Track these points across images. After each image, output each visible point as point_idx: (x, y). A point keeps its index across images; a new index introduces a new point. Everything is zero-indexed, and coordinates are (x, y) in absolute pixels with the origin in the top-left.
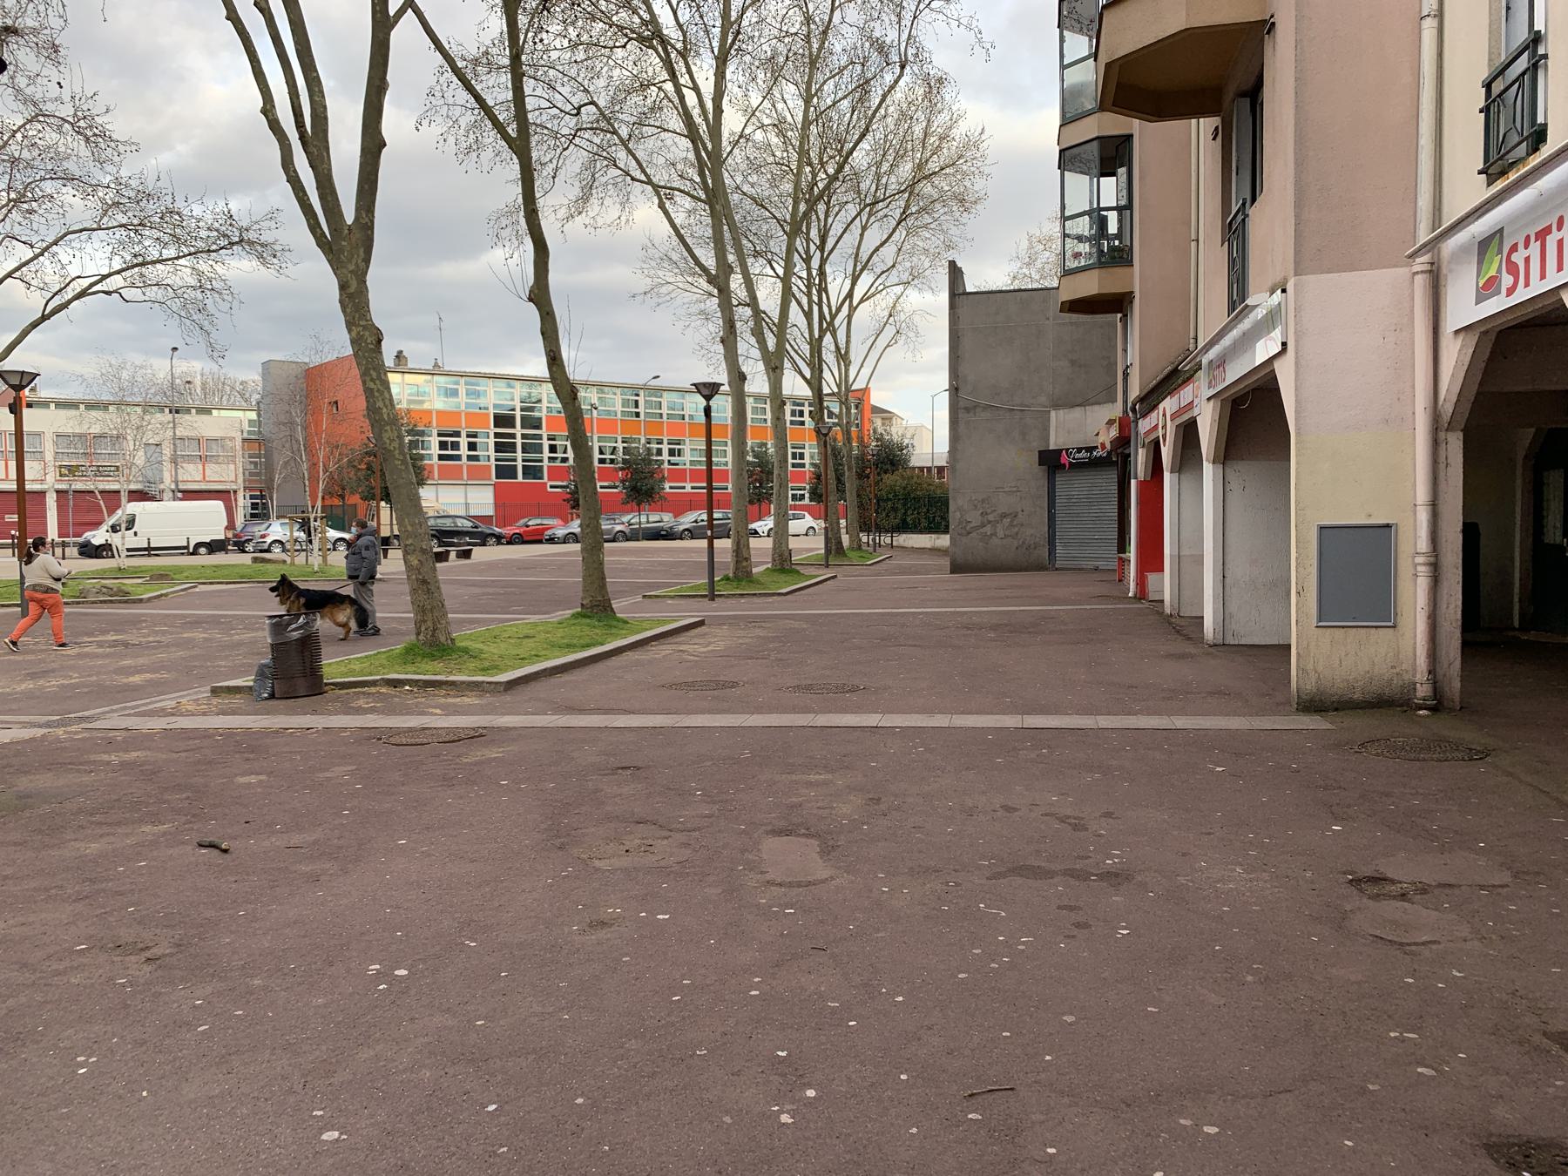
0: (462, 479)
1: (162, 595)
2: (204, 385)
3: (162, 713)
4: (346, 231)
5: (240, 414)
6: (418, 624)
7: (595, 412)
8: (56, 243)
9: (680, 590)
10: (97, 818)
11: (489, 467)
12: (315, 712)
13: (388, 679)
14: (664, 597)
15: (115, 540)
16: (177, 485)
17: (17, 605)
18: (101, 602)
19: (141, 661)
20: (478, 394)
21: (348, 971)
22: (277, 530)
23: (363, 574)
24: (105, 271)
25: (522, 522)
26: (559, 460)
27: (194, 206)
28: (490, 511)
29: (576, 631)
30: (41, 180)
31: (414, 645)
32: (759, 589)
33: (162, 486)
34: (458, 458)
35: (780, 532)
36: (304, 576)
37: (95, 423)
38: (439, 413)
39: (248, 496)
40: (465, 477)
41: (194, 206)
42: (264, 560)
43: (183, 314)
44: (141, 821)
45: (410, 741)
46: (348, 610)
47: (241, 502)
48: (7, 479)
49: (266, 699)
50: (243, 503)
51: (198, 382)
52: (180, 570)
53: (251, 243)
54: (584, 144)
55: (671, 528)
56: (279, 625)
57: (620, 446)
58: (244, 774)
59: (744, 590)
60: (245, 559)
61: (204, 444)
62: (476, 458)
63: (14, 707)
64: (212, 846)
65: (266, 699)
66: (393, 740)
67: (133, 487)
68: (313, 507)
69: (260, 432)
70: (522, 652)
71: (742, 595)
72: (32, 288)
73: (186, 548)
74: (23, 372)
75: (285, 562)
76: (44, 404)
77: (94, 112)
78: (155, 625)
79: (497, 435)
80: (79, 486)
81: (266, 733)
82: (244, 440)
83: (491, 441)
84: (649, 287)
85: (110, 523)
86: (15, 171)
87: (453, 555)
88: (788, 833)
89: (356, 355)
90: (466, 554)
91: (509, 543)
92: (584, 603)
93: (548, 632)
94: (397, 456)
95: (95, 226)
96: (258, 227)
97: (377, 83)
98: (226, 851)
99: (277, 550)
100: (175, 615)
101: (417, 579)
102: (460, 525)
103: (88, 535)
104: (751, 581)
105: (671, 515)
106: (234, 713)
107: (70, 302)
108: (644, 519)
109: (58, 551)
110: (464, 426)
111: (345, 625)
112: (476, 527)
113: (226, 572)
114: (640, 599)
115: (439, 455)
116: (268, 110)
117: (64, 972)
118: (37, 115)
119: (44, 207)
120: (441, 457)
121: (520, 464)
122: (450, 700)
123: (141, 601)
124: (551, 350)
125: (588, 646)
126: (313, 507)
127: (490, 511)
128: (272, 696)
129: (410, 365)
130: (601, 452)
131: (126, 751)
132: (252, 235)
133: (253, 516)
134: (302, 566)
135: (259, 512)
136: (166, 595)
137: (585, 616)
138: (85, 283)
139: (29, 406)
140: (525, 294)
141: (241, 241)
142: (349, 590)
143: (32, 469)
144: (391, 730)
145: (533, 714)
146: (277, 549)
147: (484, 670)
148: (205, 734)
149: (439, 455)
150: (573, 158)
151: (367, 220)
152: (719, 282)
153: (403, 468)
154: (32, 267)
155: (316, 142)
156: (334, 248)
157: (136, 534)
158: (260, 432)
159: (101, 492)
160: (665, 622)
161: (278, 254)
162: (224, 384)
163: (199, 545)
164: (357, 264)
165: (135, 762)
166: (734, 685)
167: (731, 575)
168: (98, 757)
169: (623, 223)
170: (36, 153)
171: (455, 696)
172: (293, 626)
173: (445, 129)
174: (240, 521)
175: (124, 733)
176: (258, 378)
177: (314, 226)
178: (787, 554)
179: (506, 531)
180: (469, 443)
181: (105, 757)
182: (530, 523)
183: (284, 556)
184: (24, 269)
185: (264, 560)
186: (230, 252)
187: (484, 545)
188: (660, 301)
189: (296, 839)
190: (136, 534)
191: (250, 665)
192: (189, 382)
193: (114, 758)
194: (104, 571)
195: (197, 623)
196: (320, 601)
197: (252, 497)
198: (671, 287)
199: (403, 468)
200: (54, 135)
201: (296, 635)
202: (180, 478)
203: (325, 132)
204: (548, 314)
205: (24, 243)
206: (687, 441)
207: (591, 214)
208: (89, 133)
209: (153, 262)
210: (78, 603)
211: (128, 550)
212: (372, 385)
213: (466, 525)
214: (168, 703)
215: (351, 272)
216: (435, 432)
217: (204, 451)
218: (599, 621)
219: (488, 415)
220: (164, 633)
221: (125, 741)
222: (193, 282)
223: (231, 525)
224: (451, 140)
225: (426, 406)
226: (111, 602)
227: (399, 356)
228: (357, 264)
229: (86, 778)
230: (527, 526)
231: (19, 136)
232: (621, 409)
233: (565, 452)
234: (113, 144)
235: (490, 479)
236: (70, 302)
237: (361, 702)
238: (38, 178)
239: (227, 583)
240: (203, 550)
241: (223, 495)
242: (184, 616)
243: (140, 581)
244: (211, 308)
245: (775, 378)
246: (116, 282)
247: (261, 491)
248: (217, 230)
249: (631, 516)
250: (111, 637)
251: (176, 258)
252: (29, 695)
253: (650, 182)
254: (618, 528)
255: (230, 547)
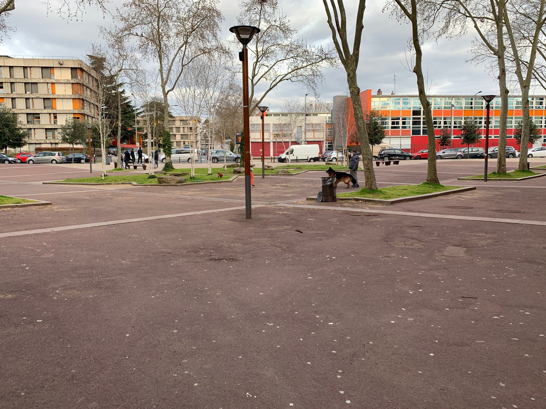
0: (399, 135)
1: (298, 173)
2: (316, 105)
3: (293, 203)
4: (350, 57)
5: (326, 115)
6: (366, 183)
7: (453, 108)
8: (274, 65)
9: (474, 177)
10: (275, 224)
11: (410, 130)
12: (332, 206)
13: (355, 199)
14: (467, 179)
15: (287, 157)
16: (306, 140)
17: (261, 175)
18: (282, 175)
19: (290, 191)
20: (406, 103)
21: (322, 256)
22: (334, 154)
23: (354, 167)
24: (286, 73)
25: (421, 151)
26: (437, 127)
27: (312, 48)
28: (409, 147)
29: (423, 188)
30: (271, 46)
31: (365, 189)
32: (507, 177)
33: (302, 140)
34: (399, 127)
35: (523, 155)
36: (341, 169)
37: (283, 120)
38: (392, 111)
39: (327, 143)
40: (401, 135)
41: (312, 48)
42: (329, 164)
43: (308, 84)
44: (284, 225)
45: (356, 215)
46: (349, 179)
47: (325, 144)
48: (260, 138)
49: (320, 202)
50: (325, 146)
51: (314, 105)
52: (304, 166)
53: (328, 59)
54: (448, 6)
55: (482, 154)
56: (324, 180)
57: (463, 121)
58: (310, 218)
59: (501, 178)
60: (324, 163)
61: (314, 126)
62: (405, 127)
63: (259, 200)
64: (299, 231)
65: (320, 202)
66: (351, 214)
67: (293, 140)
68: (344, 146)
69: (332, 121)
70: (400, 194)
71: (500, 180)
72: (268, 80)
73: (307, 160)
74: (264, 107)
75: (336, 164)
76: (271, 115)
77: (285, 22)
78: (296, 182)
79: (413, 118)
80: (278, 140)
81: (318, 210)
82: (327, 124)
83: (411, 121)
84: (474, 57)
85: (286, 152)
86: (264, 45)
87: (392, 163)
88: (459, 246)
89: (351, 97)
90: (397, 163)
91: (414, 159)
92: (428, 179)
93: (413, 188)
94: (362, 129)
95: (284, 58)
96: (331, 53)
97: (362, 7)
98: (301, 232)
99: (334, 161)
100: (301, 179)
101: (367, 168)
102: (396, 152)
103: (281, 155)
104: (505, 175)
105: (482, 148)
106: (311, 205)
107: (277, 84)
108: (470, 150)
109: (273, 160)
110: (401, 115)
111: (348, 183)
112: (402, 153)
113: (317, 167)
114: (456, 180)
115: (391, 127)
116: (329, 21)
117: (265, 249)
118: (270, 26)
119: (271, 55)
120: (392, 128)
121: (422, 129)
122: (372, 206)
123: (293, 175)
124: (420, 89)
125: (425, 193)
126: (344, 146)
127: (409, 147)
128: (322, 201)
129: (383, 94)
130: (455, 123)
131: (283, 211)
132: (329, 56)
133: (328, 149)
134: (341, 166)
135: (330, 148)
136: (299, 173)
137: (427, 184)
138: (281, 77)
139: (267, 115)
140: (412, 70)
141: (325, 58)
142: (349, 173)
143: (266, 135)
144: (354, 212)
145: (396, 211)
146: (334, 160)
147: (385, 198)
148: (303, 209)
149: (391, 127)
150: (442, 12)
151: (357, 53)
152: (500, 53)
153: (364, 132)
154: (268, 73)
155: (342, 31)
156: (346, 63)
157: (293, 155)
158: (332, 121)
159: (284, 142)
160: (459, 187)
161: (337, 61)
162: (322, 105)
163: (311, 159)
164: (353, 68)
165: (285, 214)
166: (472, 208)
167: (496, 172)
168: (277, 212)
169: (462, 34)
170: (270, 38)
171: (374, 205)
172: (328, 181)
173: (393, 10)
174: (324, 151)
175: (283, 207)
176: (332, 102)
177: (341, 57)
178: (526, 164)
179: (415, 155)
180: (403, 122)
181: (279, 212)
182: (424, 152)
183: (336, 163)
184: (266, 74)
185: (329, 164)
186: (322, 62)
187: (405, 160)
188: (479, 62)
189: (319, 232)
190: (293, 155)
191: (316, 193)
192: (311, 105)
193: (280, 213)
194: (284, 166)
195: (307, 182)
196: (341, 176)
197: (329, 143)
198: (484, 56)
199: (364, 132)
200: (274, 31)
201: (329, 183)
202: (307, 137)
203: (345, 26)
204: (420, 76)
205: (266, 66)
206: (494, 118)
207: (449, 33)
208: (284, 29)
209: (300, 69)
210: (276, 175)
211: (291, 160)
212: (356, 106)
213: (399, 152)
214: (295, 201)
215: (351, 70)
216: (390, 118)
217: (314, 128)
218: (433, 186)
219: (411, 111)
220: (298, 184)
221: (283, 209)
222: (311, 73)
223: (321, 152)
224: (395, 14)
225: (388, 109)
226: (285, 175)
227: (379, 91)
228: (353, 68)
229: (274, 216)
230: (423, 153)
231: (265, 33)
232: (464, 106)
233: (440, 124)
234: (290, 32)
235: (410, 135)
236: (277, 84)
237: (346, 204)
238: (270, 46)
239: (317, 171)
240: (312, 160)
241: (319, 143)
242: (304, 180)
243: (293, 169)
244: (316, 81)
245: (525, 91)
246: (289, 76)
247: (331, 141)
248: (318, 55)
249: (465, 149)
250: (284, 184)
251: (306, 66)
252: (263, 197)
253: (470, 16)
254: (459, 153)
255: (320, 160)
